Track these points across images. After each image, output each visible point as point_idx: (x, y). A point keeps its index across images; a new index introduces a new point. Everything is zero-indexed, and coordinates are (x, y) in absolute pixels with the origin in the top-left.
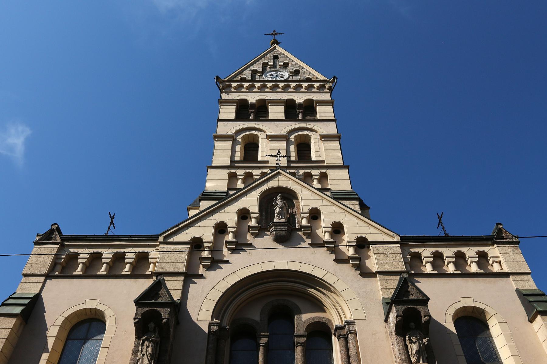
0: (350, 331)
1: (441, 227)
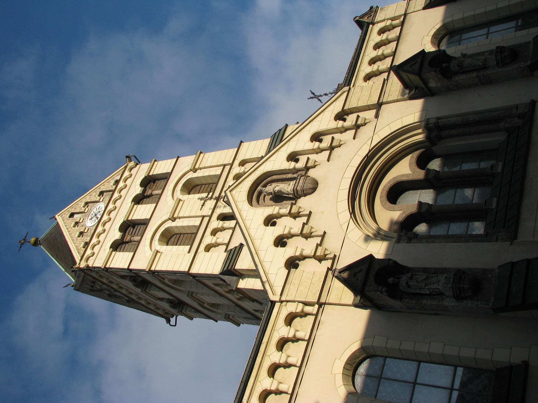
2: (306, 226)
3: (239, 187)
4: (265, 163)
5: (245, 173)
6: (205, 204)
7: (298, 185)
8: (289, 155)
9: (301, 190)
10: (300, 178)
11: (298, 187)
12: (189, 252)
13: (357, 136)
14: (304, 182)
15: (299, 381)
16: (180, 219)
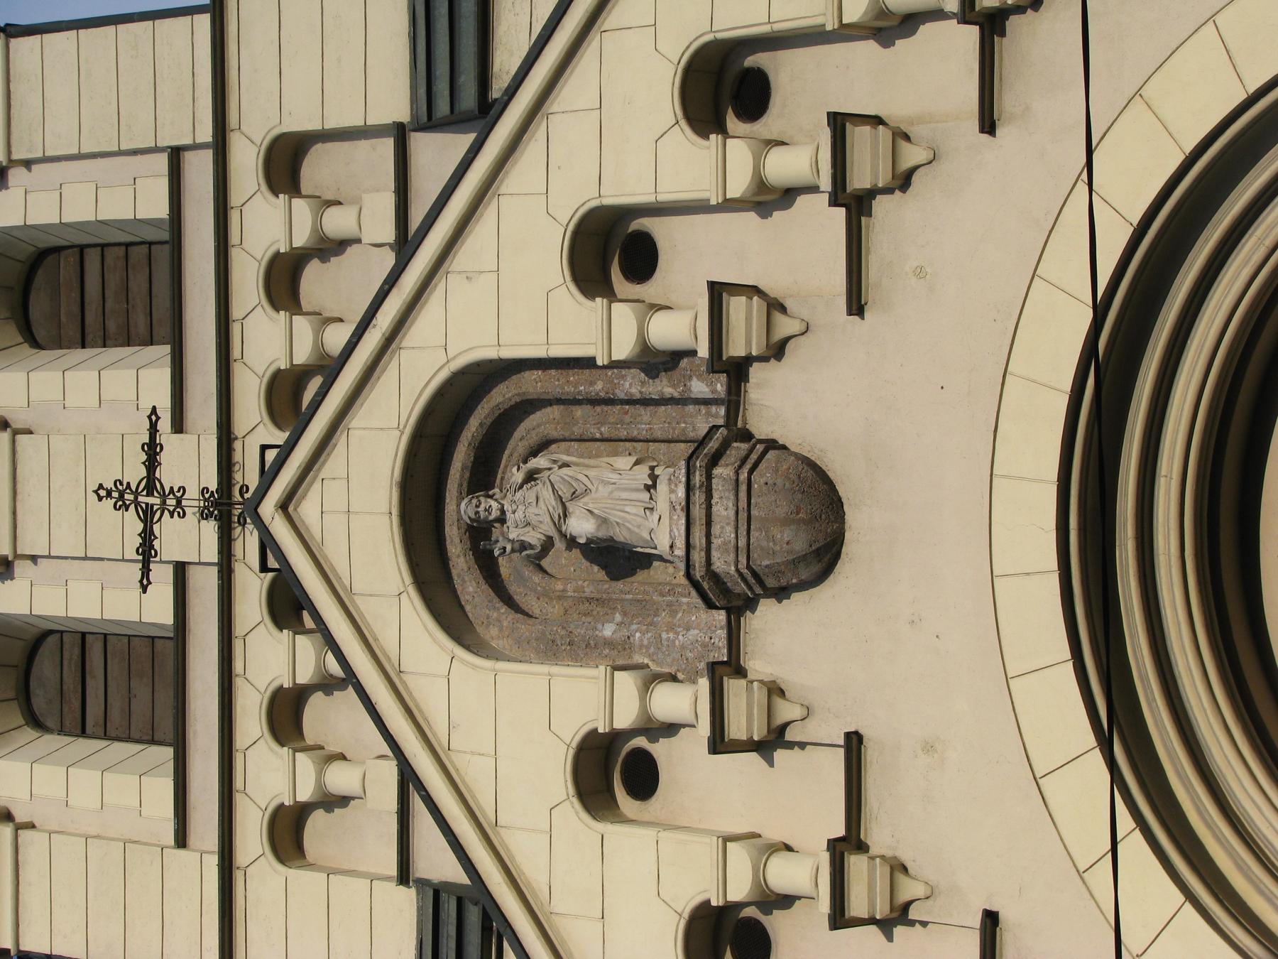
2: (856, 864)
3: (316, 531)
4: (441, 287)
5: (330, 368)
6: (156, 543)
7: (708, 535)
8: (576, 234)
9: (741, 574)
10: (709, 477)
11: (715, 554)
12: (181, 840)
13: (1007, 101)
14: (743, 516)
15: (1226, 343)
16: (34, 167)
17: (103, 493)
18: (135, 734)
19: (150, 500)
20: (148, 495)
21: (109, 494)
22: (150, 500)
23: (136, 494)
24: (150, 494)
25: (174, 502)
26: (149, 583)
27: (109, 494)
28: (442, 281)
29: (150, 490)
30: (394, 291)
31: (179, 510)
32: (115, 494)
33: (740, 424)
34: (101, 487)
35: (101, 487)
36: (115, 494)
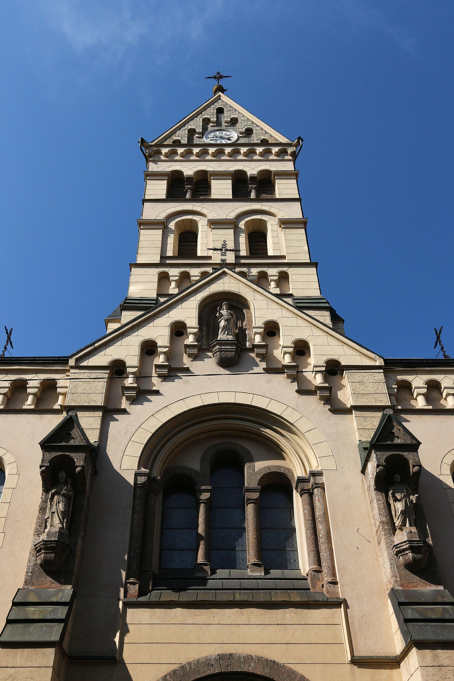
0: (316, 484)
1: (439, 347)
17: (225, 242)
18: (266, 245)
19: (224, 250)
20: (225, 250)
21: (225, 243)
22: (224, 250)
23: (225, 248)
24: (225, 250)
25: (224, 254)
26: (209, 250)
27: (225, 243)
28: (357, 354)
29: (226, 250)
30: (264, 291)
31: (222, 255)
32: (224, 244)
33: (226, 323)
34: (226, 242)
35: (226, 242)
36: (224, 244)
